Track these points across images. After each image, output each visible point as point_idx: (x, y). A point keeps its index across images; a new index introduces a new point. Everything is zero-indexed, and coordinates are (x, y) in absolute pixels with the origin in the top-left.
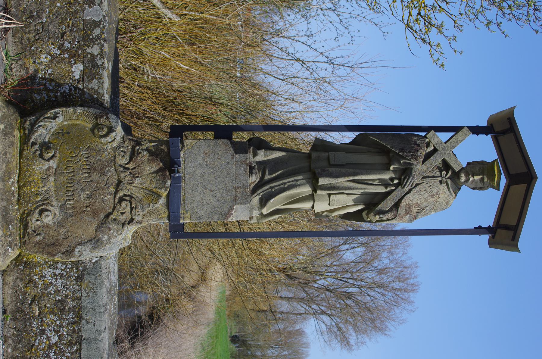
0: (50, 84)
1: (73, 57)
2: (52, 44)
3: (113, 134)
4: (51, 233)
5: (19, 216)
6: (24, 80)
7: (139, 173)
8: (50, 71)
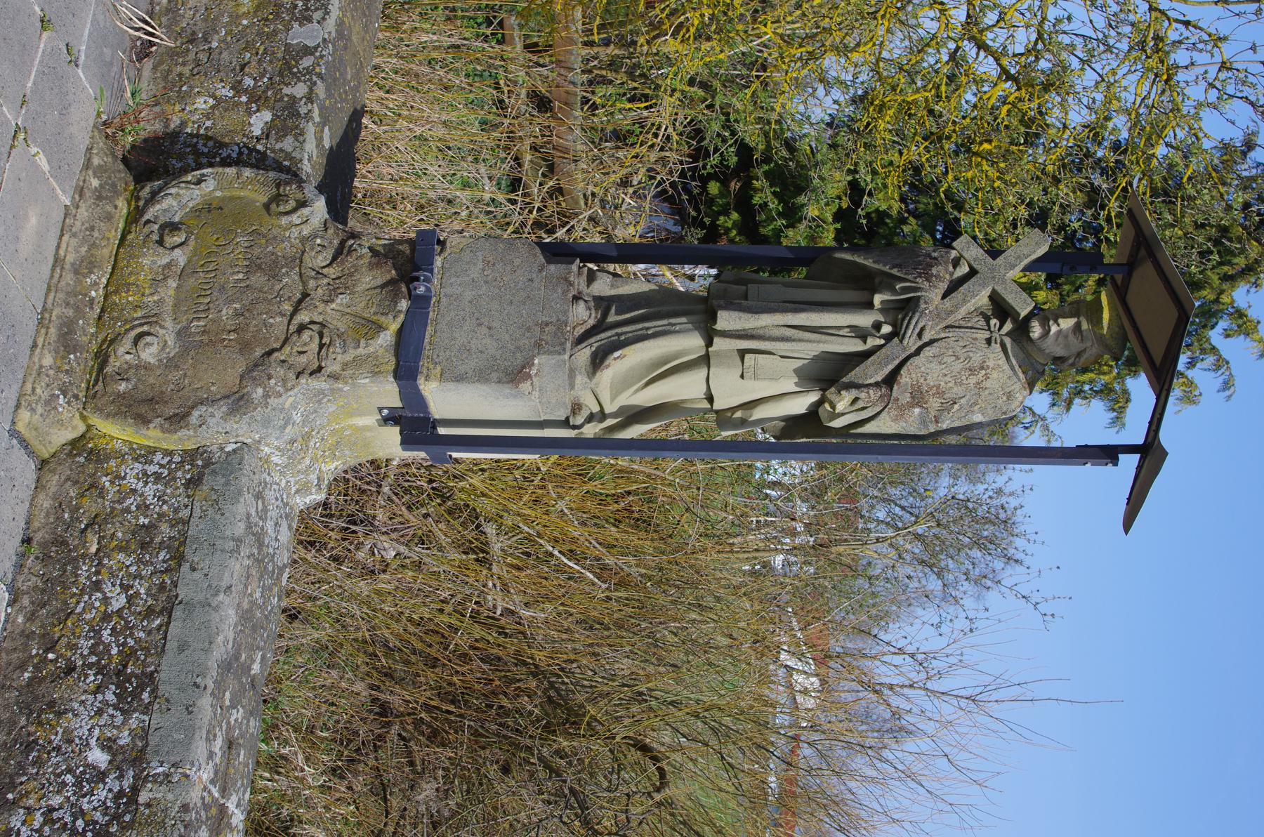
0: (205, 145)
1: (255, 102)
2: (222, 81)
3: (306, 211)
4: (151, 380)
5: (94, 348)
6: (157, 138)
8: (208, 124)
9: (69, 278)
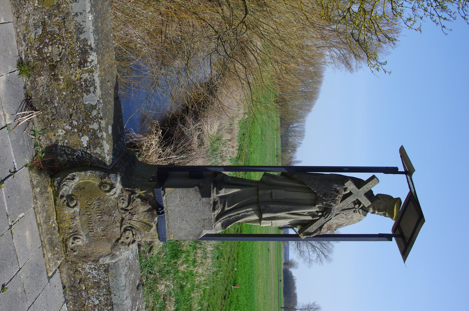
0: (68, 150)
2: (65, 122)
3: (114, 190)
4: (83, 250)
6: (50, 147)
7: (135, 212)
8: (66, 141)
9: (45, 227)
